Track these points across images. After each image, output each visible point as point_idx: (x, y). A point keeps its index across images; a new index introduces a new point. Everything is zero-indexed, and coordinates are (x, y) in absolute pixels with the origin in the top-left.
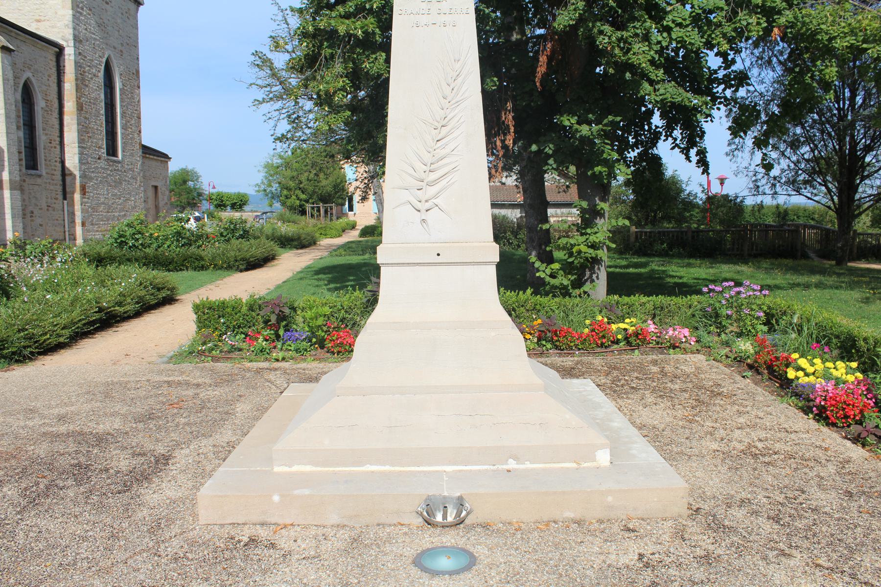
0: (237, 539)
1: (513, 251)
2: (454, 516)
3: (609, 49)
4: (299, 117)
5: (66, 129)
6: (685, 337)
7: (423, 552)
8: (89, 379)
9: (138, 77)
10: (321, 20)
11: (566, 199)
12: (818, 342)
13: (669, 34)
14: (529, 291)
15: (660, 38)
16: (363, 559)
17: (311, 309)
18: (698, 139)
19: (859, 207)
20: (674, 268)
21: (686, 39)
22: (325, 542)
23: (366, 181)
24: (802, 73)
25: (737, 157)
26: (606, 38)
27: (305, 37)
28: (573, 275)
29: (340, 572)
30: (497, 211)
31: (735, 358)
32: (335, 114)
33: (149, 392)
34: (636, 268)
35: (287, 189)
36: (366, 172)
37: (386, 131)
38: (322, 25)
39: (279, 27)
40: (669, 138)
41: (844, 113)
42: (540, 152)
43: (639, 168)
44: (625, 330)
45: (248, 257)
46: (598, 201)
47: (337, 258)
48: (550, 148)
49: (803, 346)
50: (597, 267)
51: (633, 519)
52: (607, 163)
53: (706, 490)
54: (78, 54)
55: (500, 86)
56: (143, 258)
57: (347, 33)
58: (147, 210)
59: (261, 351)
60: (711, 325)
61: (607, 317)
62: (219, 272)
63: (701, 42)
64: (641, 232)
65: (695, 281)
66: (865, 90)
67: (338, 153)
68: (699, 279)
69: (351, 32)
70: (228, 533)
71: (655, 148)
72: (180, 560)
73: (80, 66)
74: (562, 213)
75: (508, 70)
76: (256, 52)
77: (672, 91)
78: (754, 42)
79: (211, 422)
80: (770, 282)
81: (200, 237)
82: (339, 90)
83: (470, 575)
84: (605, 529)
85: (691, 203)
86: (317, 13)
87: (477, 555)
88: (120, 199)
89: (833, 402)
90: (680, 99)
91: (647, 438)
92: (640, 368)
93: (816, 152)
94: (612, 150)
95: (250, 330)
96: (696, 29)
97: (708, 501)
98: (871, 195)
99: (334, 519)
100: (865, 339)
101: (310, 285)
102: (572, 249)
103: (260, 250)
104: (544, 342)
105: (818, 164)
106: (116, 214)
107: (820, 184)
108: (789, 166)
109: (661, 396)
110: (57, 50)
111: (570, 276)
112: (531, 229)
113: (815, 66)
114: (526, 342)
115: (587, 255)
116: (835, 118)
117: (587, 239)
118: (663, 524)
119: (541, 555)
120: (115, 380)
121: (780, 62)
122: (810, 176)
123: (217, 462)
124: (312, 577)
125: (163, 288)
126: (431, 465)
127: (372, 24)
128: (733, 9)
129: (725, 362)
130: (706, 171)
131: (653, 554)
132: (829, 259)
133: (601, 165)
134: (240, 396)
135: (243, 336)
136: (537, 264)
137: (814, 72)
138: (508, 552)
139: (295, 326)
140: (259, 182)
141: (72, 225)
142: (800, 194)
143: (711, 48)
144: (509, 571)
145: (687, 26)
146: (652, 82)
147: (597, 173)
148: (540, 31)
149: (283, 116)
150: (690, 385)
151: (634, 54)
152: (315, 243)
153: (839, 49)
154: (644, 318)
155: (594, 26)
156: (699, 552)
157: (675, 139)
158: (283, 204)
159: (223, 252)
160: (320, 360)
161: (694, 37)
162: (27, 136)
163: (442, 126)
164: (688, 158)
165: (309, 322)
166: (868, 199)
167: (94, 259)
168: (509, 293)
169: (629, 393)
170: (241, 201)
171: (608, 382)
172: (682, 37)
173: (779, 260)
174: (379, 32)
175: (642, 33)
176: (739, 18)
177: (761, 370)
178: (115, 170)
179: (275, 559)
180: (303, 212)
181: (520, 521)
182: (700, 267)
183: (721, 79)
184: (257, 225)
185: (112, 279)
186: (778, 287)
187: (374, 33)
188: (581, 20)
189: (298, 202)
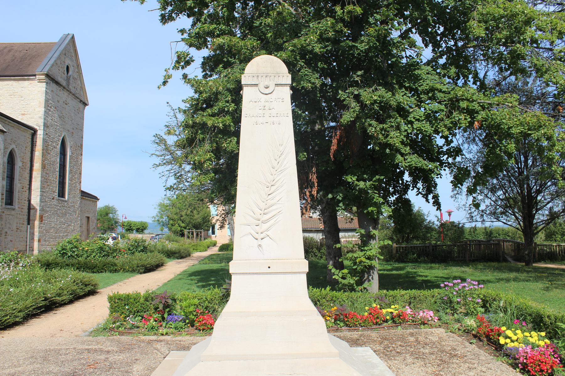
4: (181, 175)
5: (33, 180)
6: (431, 317)
8: (33, 347)
9: (82, 149)
10: (197, 117)
12: (518, 319)
13: (412, 126)
15: (406, 128)
17: (186, 300)
18: (433, 189)
19: (536, 228)
20: (422, 270)
21: (423, 128)
23: (223, 216)
24: (494, 148)
25: (458, 198)
26: (374, 128)
27: (187, 127)
28: (356, 277)
30: (307, 235)
31: (464, 331)
34: (397, 271)
35: (173, 220)
36: (223, 210)
37: (236, 186)
38: (198, 121)
39: (171, 120)
40: (415, 189)
41: (521, 170)
42: (334, 198)
44: (392, 313)
45: (145, 264)
46: (371, 229)
48: (340, 196)
49: (508, 321)
50: (372, 271)
52: (376, 205)
54: (46, 134)
55: (308, 159)
56: (77, 264)
57: (213, 126)
58: (82, 232)
59: (152, 328)
60: (447, 309)
62: (126, 273)
63: (431, 130)
64: (400, 247)
65: (436, 279)
66: (533, 157)
67: (206, 198)
68: (438, 277)
69: (216, 125)
71: (406, 195)
73: (46, 142)
74: (349, 236)
75: (313, 148)
76: (156, 134)
77: (415, 160)
78: (463, 130)
80: (484, 278)
81: (115, 251)
82: (207, 160)
85: (430, 227)
86: (194, 113)
88: (64, 225)
89: (532, 361)
90: (421, 165)
92: (402, 338)
93: (507, 195)
94: (380, 197)
95: (145, 314)
96: (428, 122)
98: (543, 221)
100: (548, 317)
101: (185, 283)
102: (355, 260)
103: (155, 260)
104: (338, 322)
105: (509, 202)
106: (61, 235)
107: (511, 214)
108: (490, 203)
110: (33, 132)
111: (354, 278)
112: (329, 247)
113: (501, 143)
116: (516, 173)
117: (365, 254)
120: (52, 348)
121: (480, 140)
122: (504, 209)
125: (89, 285)
127: (228, 120)
128: (449, 111)
129: (458, 333)
130: (439, 208)
132: (521, 262)
133: (373, 206)
134: (137, 360)
135: (140, 318)
136: (333, 270)
137: (501, 147)
139: (175, 312)
140: (155, 215)
141: (32, 241)
142: (499, 221)
145: (422, 121)
146: (402, 155)
147: (370, 211)
148: (332, 124)
150: (436, 350)
151: (391, 138)
152: (189, 255)
153: (514, 134)
154: (403, 305)
155: (365, 122)
157: (419, 189)
158: (170, 229)
160: (191, 334)
161: (427, 127)
162: (8, 184)
163: (272, 186)
164: (427, 201)
165: (184, 309)
166: (541, 223)
167: (45, 264)
168: (315, 290)
170: (143, 227)
171: (382, 348)
172: (420, 127)
173: (489, 263)
176: (453, 116)
177: (482, 338)
178: (63, 206)
180: (183, 235)
183: (445, 152)
184: (152, 243)
185: (55, 278)
186: (489, 281)
187: (230, 126)
188: (358, 118)
189: (179, 228)
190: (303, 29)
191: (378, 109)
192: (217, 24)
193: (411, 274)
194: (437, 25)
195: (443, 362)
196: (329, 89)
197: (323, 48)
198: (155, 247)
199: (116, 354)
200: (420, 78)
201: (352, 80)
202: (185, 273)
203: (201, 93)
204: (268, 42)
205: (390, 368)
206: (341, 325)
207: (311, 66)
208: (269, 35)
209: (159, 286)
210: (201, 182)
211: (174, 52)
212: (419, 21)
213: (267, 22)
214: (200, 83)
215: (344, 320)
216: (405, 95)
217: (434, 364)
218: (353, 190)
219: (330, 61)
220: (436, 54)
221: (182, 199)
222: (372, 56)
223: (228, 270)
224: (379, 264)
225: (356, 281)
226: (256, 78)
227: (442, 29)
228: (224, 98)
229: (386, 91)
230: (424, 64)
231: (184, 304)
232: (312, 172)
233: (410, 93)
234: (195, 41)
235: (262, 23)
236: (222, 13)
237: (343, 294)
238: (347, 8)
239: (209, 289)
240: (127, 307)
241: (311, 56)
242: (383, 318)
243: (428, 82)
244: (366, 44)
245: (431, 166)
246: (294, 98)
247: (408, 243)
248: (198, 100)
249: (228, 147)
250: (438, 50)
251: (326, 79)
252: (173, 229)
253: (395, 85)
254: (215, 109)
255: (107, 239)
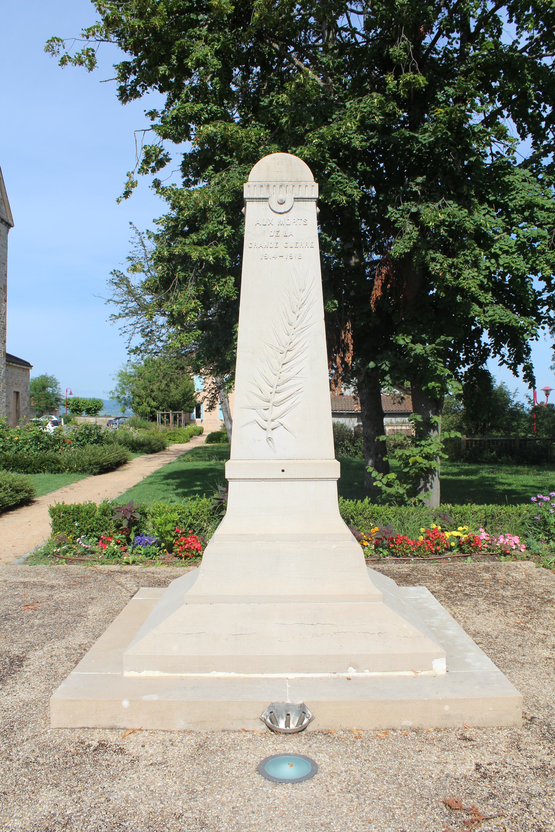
0: (87, 743)
1: (350, 458)
2: (296, 723)
3: (440, 274)
4: (152, 331)
6: (515, 544)
7: (267, 760)
9: (6, 292)
10: (176, 247)
11: (401, 409)
13: (497, 261)
14: (367, 500)
15: (488, 264)
16: (208, 766)
17: (160, 515)
18: (524, 356)
20: (503, 475)
21: (513, 265)
22: (172, 747)
23: (213, 392)
26: (438, 265)
28: (408, 484)
29: (186, 779)
30: (336, 420)
32: (186, 332)
33: (6, 592)
35: (139, 396)
36: (213, 383)
38: (176, 252)
39: (136, 249)
40: (498, 355)
42: (377, 368)
43: (469, 383)
44: (458, 537)
45: (101, 461)
47: (185, 463)
48: (386, 365)
51: (470, 728)
52: (442, 380)
53: (540, 698)
55: (340, 309)
56: (3, 460)
57: (200, 259)
58: (9, 414)
59: (113, 554)
60: (540, 533)
61: (441, 525)
62: (74, 474)
63: (526, 267)
64: (472, 441)
65: (524, 488)
68: (527, 486)
69: (203, 258)
70: (78, 737)
71: (484, 364)
72: (31, 764)
74: (397, 422)
75: (347, 293)
76: (115, 271)
79: (63, 625)
81: (57, 441)
83: (312, 784)
84: (442, 737)
85: (518, 412)
86: (171, 239)
87: (319, 763)
90: (508, 320)
91: (481, 645)
92: (473, 575)
94: (445, 367)
95: (103, 533)
96: (522, 256)
97: (542, 709)
99: (181, 725)
101: (159, 489)
104: (381, 549)
109: (493, 603)
111: (405, 485)
112: (369, 439)
114: (363, 548)
115: (421, 465)
117: (421, 451)
118: (499, 733)
119: (381, 764)
123: (69, 664)
124: (159, 784)
125: (21, 490)
126: (273, 672)
127: (222, 250)
130: (532, 385)
131: (490, 764)
134: (92, 599)
135: (96, 539)
136: (374, 474)
138: (349, 761)
139: (145, 531)
140: (113, 389)
143: (535, 273)
144: (349, 780)
145: (513, 253)
146: (481, 305)
147: (431, 388)
148: (376, 257)
149: (137, 330)
151: (464, 279)
152: (164, 448)
155: (426, 254)
156: (535, 763)
157: (503, 356)
158: (135, 410)
159: (78, 456)
160: (168, 564)
161: (520, 264)
163: (288, 351)
164: (516, 373)
169: (462, 600)
170: (96, 406)
171: (443, 588)
174: (229, 258)
175: (472, 260)
179: (124, 764)
180: (154, 419)
181: (360, 728)
182: (528, 474)
183: (545, 301)
184: (111, 431)
187: (224, 259)
188: (415, 248)
189: (149, 409)
190: (336, 111)
191: (446, 234)
192: (205, 103)
193: (488, 481)
194: (542, 104)
195: (531, 609)
196: (373, 204)
197: (366, 141)
198: (114, 435)
199: (63, 590)
200: (512, 187)
201: (408, 190)
202: (159, 474)
203: (181, 209)
204: (282, 131)
205: (454, 617)
206: (384, 553)
207: (347, 168)
208: (284, 120)
209: (121, 493)
210: (182, 343)
211: (140, 147)
212: (514, 97)
213: (280, 100)
214: (180, 194)
215: (389, 546)
216: (487, 213)
217: (518, 612)
218: (405, 356)
219: (376, 160)
220: (538, 149)
221: (153, 366)
222: (439, 153)
223: (223, 473)
224: (442, 465)
225: (407, 490)
226: (265, 188)
227: (549, 109)
228: (216, 218)
229: (460, 207)
230: (519, 166)
231: (158, 520)
232: (346, 329)
233: (496, 211)
234: (171, 130)
235: (272, 101)
236: (211, 85)
237: (388, 510)
238: (404, 77)
239: (194, 499)
240: (76, 524)
241: (347, 153)
242: (445, 545)
243: (524, 193)
244: (430, 134)
245: (522, 322)
246: (321, 219)
247: (484, 435)
248: (176, 220)
249: (222, 290)
250: (542, 142)
251: (368, 188)
252: (140, 410)
253: (473, 199)
254: (203, 234)
255: (44, 424)
